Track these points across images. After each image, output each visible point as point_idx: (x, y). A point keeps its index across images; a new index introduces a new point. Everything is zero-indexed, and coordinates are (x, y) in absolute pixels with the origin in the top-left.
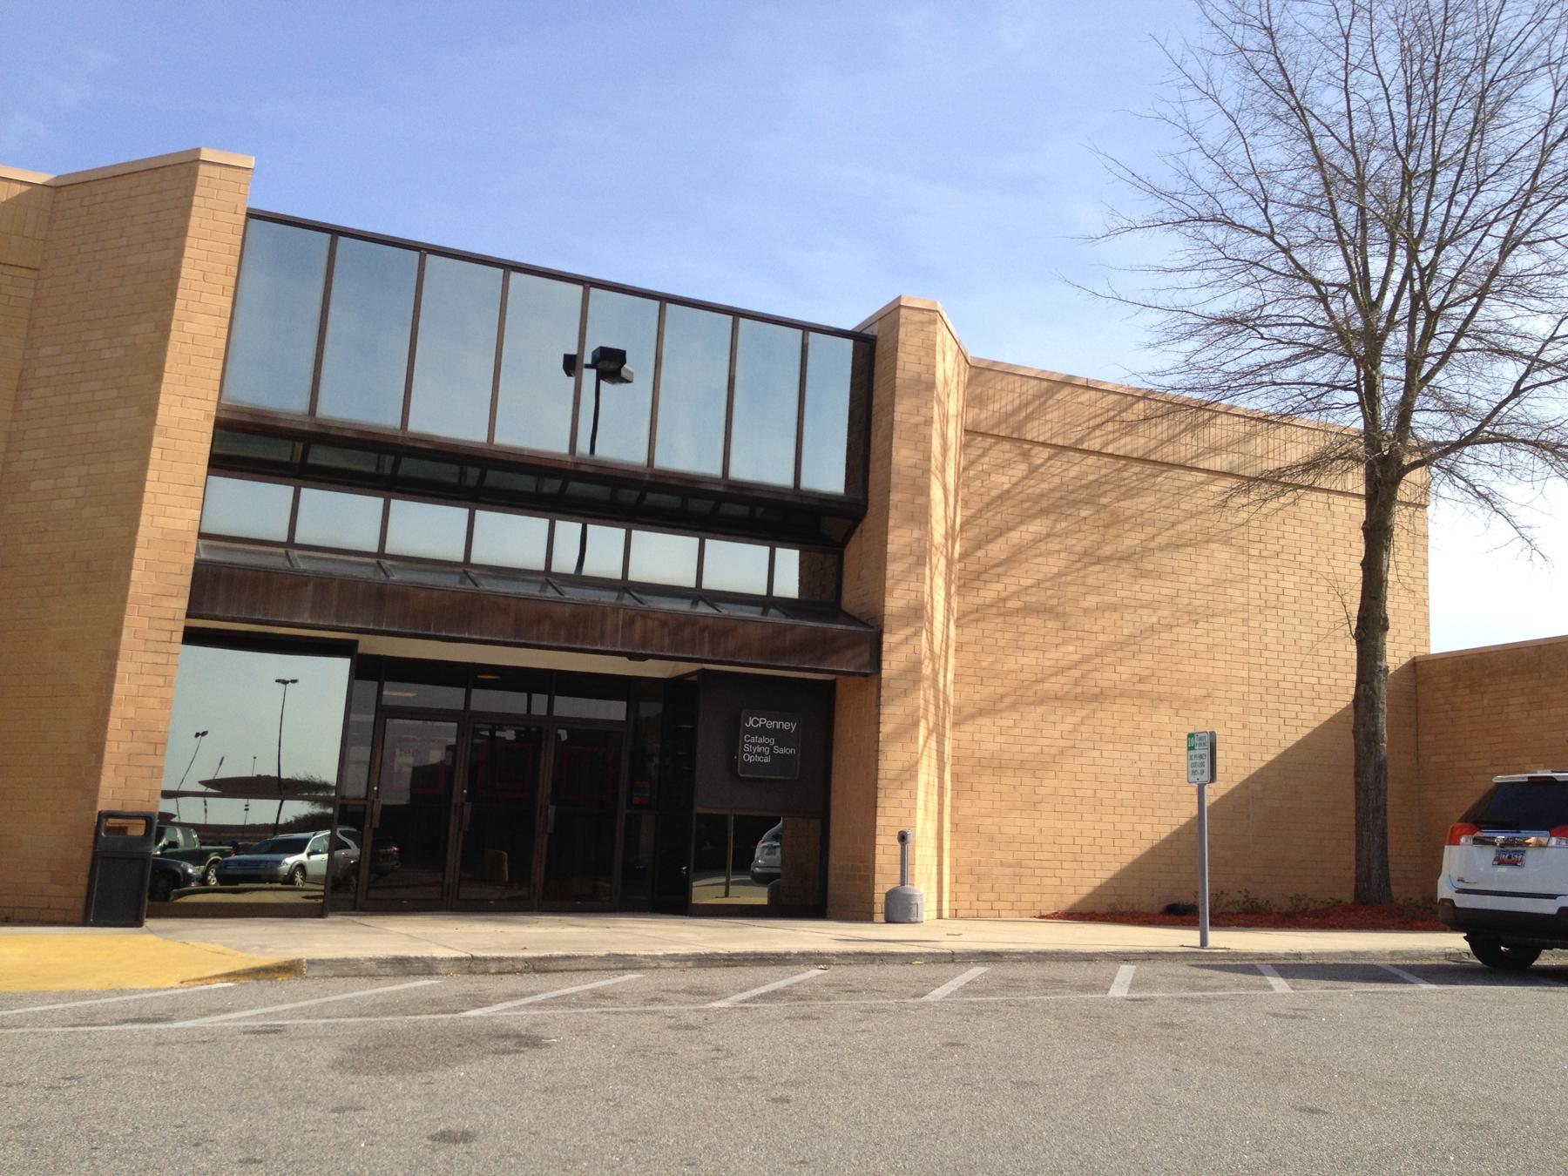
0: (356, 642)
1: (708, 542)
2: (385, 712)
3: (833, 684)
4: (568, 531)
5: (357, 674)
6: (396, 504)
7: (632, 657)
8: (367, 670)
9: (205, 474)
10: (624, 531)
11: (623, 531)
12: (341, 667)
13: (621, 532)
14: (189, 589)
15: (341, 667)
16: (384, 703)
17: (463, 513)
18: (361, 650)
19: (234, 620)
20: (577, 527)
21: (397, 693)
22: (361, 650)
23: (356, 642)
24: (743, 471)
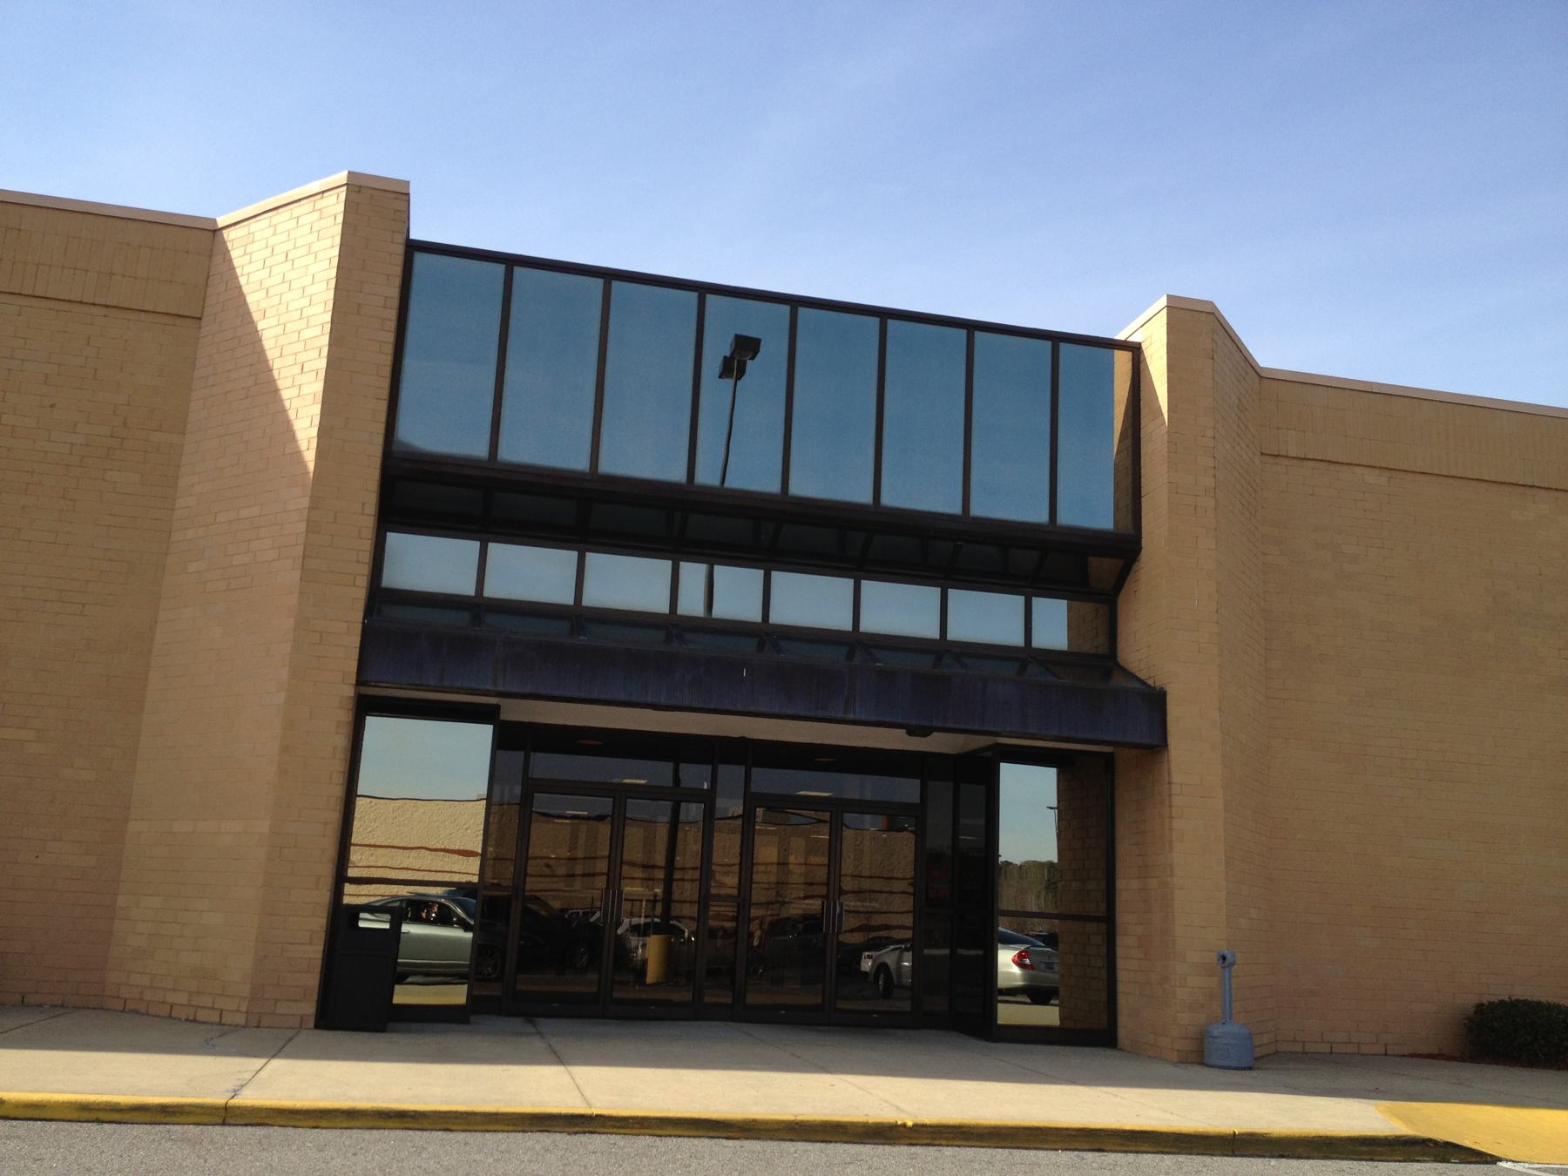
0: (497, 707)
1: (717, 568)
2: (532, 786)
3: (1108, 760)
4: (693, 573)
5: (499, 744)
6: (592, 558)
7: (912, 731)
8: (509, 739)
9: (368, 522)
10: (575, 554)
11: (477, 544)
12: (480, 736)
13: (667, 565)
14: (358, 650)
15: (480, 736)
16: (753, 789)
17: (473, 546)
18: (504, 716)
19: (1067, 740)
20: (702, 568)
21: (547, 765)
22: (504, 716)
23: (497, 707)
24: (615, 463)
